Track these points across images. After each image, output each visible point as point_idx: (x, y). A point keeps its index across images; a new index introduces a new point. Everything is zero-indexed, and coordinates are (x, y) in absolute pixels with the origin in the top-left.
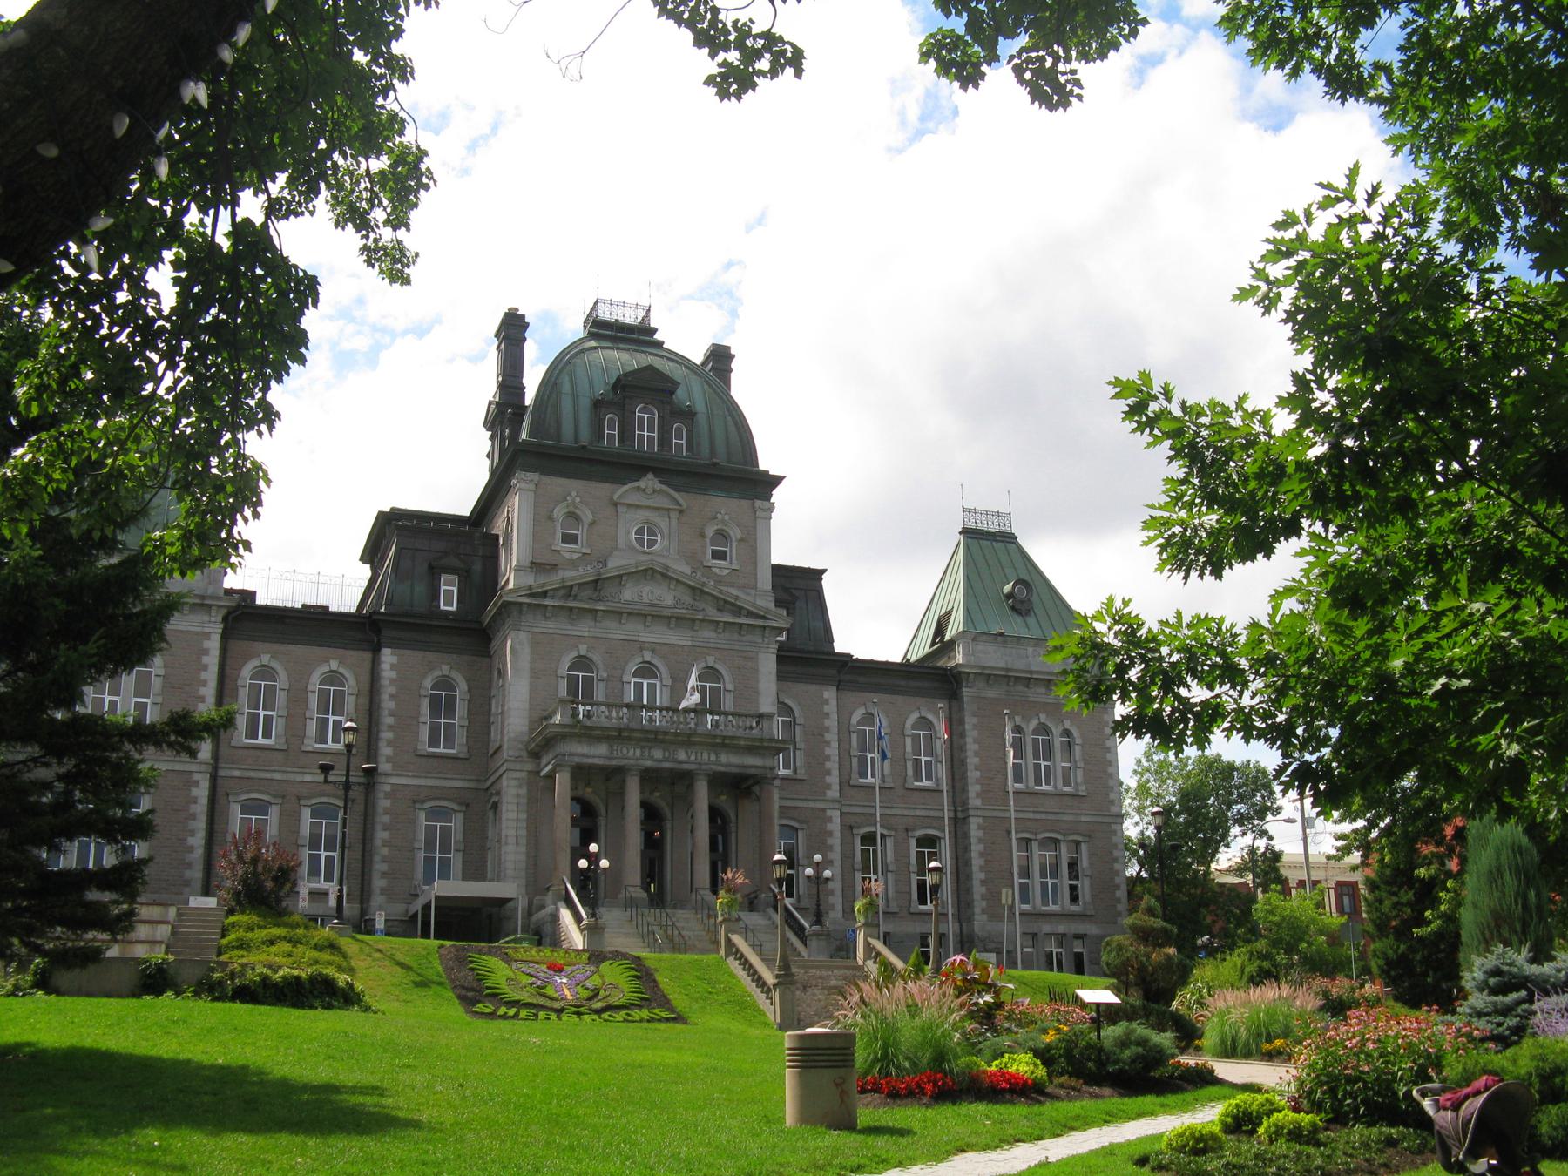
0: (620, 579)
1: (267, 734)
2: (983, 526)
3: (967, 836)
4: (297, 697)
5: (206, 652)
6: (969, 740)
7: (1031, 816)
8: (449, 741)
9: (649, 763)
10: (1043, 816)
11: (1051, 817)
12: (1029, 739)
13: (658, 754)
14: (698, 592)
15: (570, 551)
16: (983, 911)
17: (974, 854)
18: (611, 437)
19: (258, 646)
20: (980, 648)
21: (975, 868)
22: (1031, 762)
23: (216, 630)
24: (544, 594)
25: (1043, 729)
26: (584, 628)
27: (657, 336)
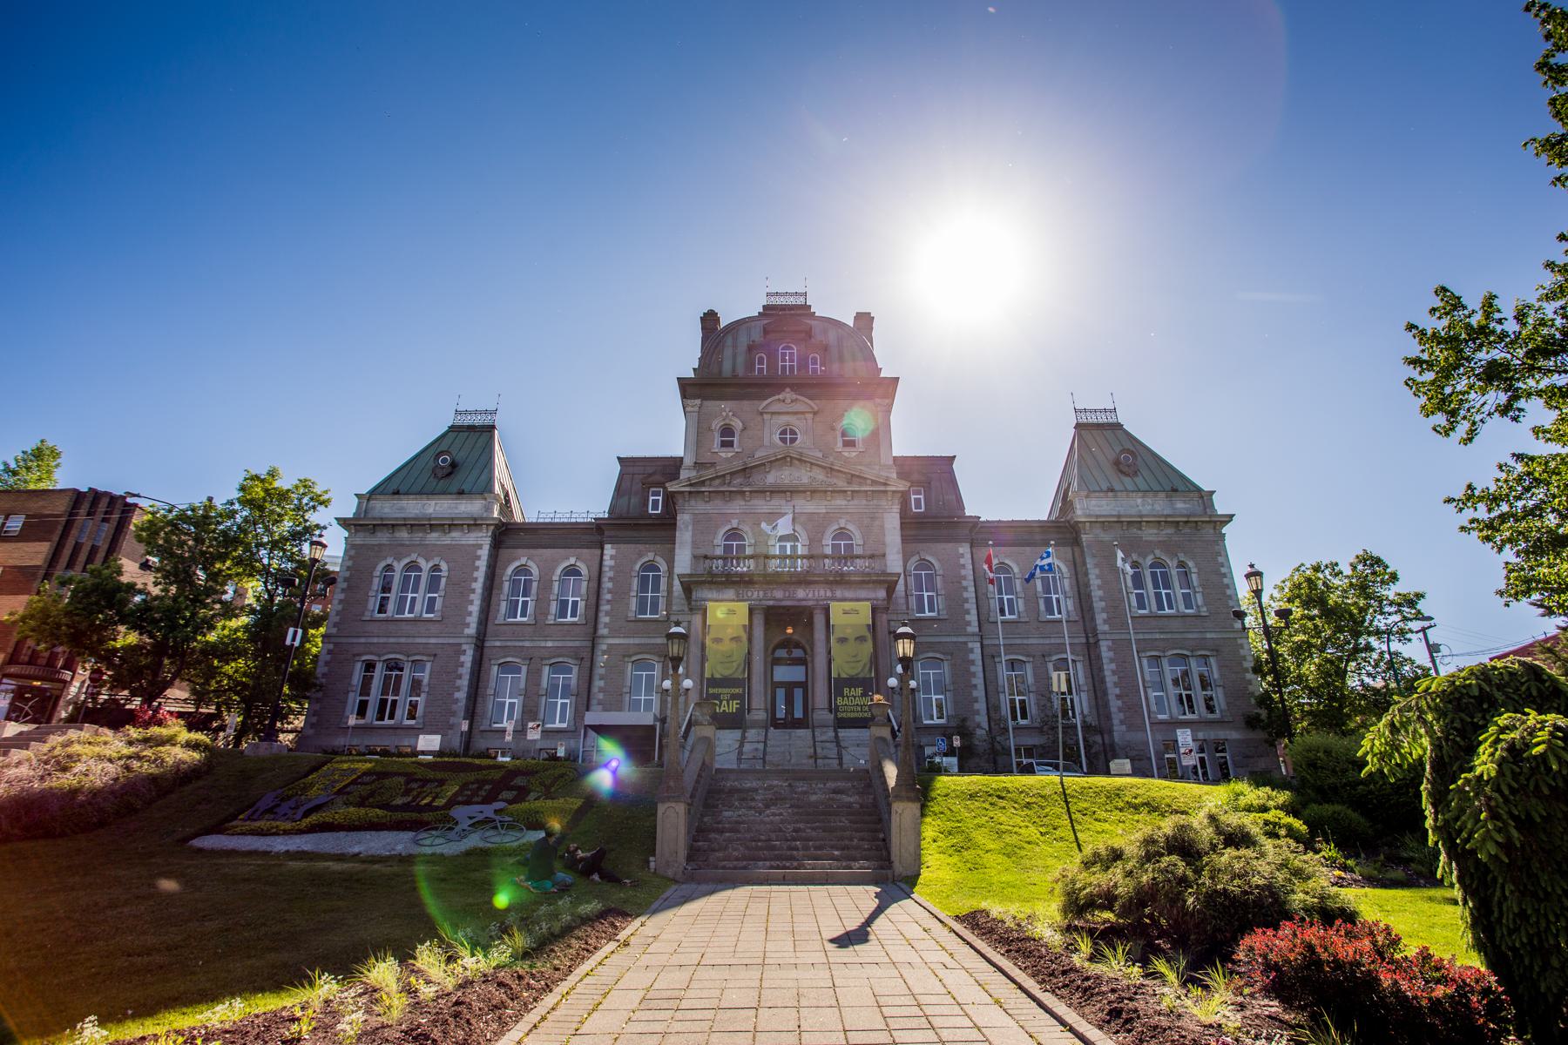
1: (1024, 716)
2: (1092, 419)
3: (1099, 657)
4: (545, 584)
5: (479, 558)
6: (1092, 576)
8: (655, 610)
12: (1147, 573)
13: (779, 594)
15: (726, 454)
16: (1122, 722)
17: (1107, 673)
18: (761, 370)
19: (520, 551)
21: (1109, 685)
23: (486, 543)
24: (703, 483)
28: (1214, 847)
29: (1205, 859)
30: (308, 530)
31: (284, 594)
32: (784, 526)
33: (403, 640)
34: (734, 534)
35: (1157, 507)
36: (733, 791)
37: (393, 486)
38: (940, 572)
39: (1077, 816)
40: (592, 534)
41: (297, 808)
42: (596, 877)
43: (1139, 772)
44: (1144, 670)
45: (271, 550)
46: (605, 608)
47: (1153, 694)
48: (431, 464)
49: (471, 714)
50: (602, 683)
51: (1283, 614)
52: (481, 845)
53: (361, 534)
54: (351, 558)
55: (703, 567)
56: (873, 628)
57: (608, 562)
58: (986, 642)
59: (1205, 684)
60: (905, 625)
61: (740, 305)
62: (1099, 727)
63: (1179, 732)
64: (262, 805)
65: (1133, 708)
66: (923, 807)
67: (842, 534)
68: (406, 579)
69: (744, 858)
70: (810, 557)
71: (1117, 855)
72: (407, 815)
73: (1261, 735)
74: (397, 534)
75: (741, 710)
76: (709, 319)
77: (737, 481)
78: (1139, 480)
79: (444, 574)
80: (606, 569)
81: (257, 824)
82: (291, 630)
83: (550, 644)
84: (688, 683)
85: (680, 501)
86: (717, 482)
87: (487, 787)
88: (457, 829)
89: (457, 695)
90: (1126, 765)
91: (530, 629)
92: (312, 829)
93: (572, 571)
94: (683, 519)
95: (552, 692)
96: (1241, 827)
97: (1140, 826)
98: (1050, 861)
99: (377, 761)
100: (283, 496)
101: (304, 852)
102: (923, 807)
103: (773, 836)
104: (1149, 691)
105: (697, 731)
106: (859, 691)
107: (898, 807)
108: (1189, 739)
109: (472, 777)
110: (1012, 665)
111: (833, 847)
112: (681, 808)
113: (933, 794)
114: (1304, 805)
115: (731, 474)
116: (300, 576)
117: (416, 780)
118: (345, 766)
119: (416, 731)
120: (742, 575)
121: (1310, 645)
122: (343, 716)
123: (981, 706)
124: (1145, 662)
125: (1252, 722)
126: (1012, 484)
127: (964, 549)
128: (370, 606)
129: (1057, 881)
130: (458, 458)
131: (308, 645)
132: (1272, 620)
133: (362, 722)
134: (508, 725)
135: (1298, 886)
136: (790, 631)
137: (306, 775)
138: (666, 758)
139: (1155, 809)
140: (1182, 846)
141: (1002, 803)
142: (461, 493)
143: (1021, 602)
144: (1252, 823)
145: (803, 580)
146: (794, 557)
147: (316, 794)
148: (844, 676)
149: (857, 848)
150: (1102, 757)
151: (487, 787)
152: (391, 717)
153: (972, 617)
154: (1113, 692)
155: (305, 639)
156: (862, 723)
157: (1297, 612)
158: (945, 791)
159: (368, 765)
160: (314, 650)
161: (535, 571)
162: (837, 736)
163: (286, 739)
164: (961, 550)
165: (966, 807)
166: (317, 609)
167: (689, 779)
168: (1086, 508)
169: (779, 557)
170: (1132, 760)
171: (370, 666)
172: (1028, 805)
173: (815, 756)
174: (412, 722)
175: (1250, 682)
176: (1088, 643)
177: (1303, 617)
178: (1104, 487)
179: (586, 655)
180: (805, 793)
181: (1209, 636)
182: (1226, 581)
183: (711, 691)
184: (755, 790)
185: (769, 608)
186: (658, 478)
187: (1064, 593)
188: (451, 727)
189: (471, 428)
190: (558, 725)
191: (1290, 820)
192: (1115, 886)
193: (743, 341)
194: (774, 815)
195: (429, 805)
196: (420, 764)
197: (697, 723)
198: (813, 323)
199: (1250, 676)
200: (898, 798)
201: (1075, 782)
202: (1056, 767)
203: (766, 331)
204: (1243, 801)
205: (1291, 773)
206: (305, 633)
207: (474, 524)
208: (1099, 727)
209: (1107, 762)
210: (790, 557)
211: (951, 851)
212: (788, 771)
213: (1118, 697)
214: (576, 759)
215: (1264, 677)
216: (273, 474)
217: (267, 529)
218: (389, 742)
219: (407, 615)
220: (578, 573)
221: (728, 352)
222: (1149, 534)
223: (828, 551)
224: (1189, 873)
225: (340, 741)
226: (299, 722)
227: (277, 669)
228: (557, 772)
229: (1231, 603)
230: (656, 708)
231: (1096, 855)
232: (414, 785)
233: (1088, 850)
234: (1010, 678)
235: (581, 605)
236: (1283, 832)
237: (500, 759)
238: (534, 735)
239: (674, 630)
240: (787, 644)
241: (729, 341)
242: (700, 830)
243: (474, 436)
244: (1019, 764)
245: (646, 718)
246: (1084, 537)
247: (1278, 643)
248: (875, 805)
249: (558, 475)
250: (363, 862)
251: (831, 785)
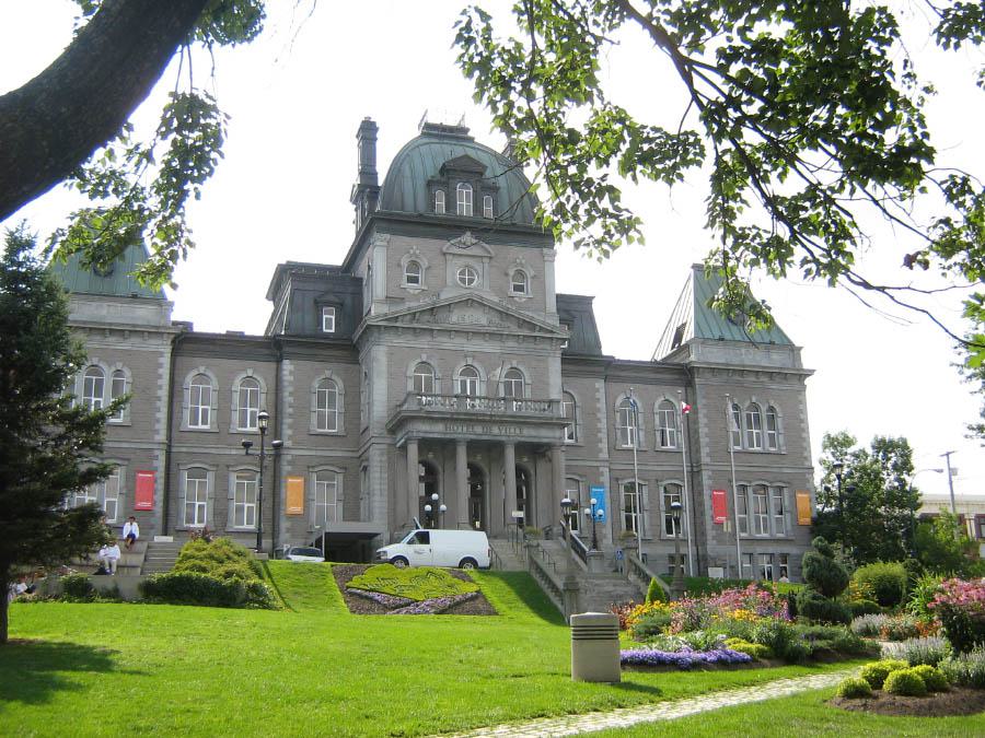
0: (449, 307)
3: (700, 484)
6: (700, 415)
13: (479, 429)
14: (505, 315)
16: (714, 538)
19: (197, 360)
23: (167, 350)
26: (424, 342)
27: (470, 134)
83: (234, 452)
136: (525, 460)
164: (597, 385)
182: (806, 454)
185: (519, 442)
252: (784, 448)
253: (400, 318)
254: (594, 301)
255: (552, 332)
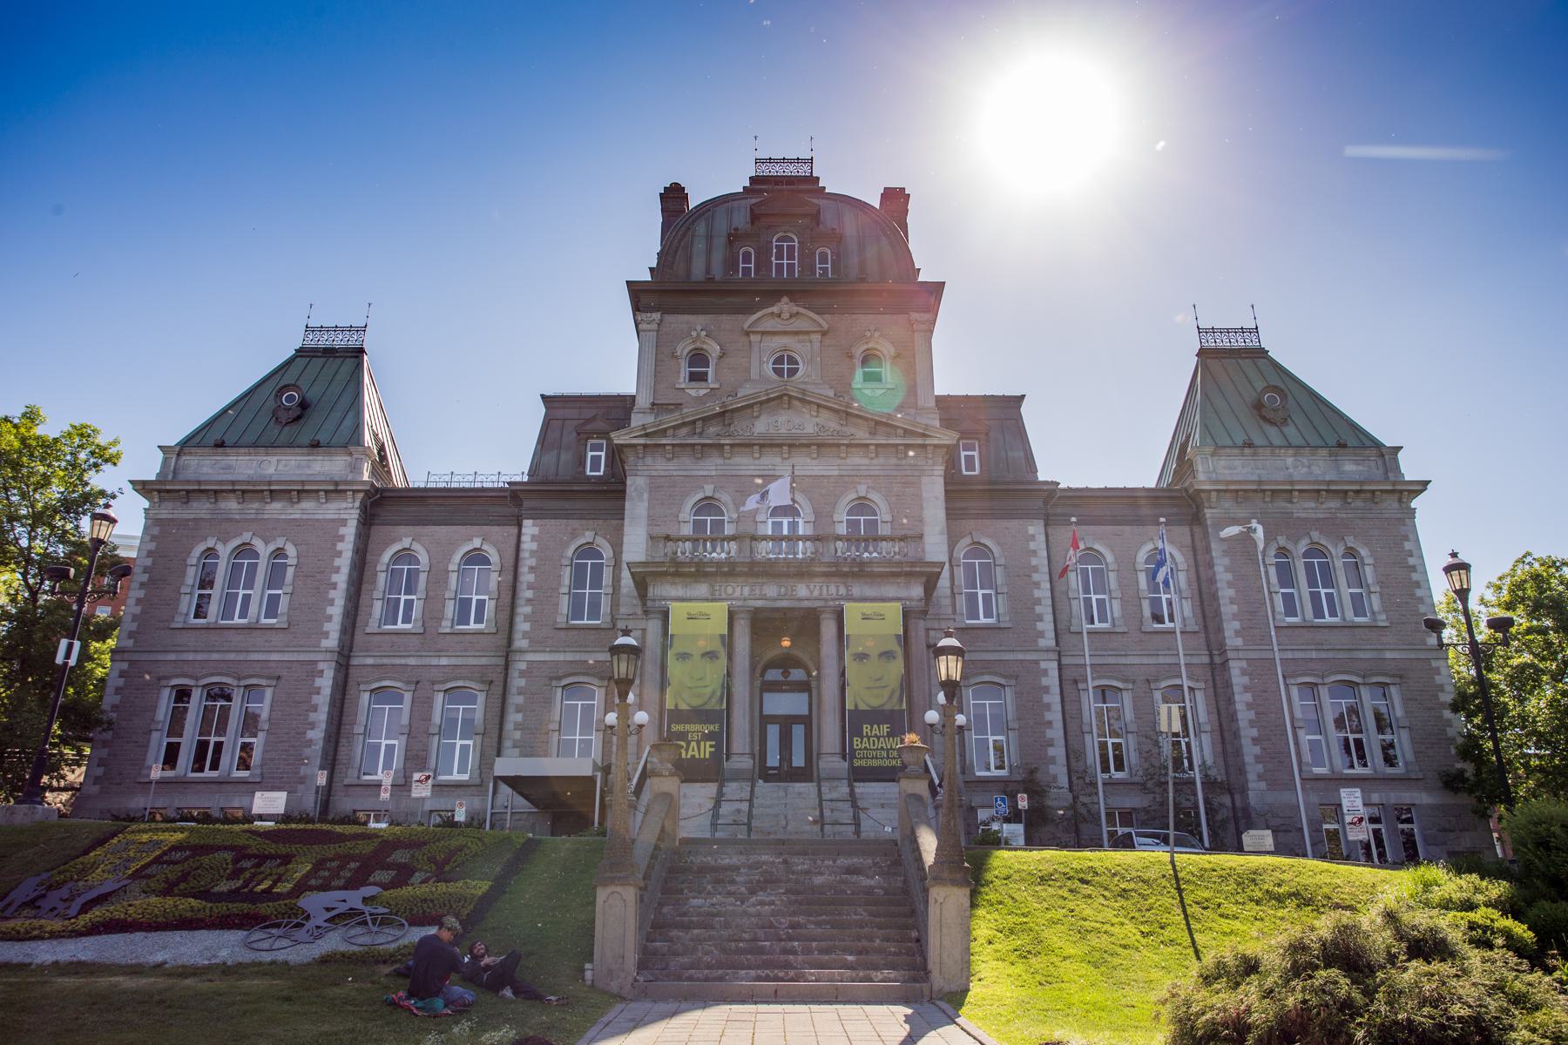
1: (1119, 766)
2: (1224, 342)
3: (1228, 684)
4: (438, 576)
5: (342, 538)
6: (1219, 569)
7: (1314, 655)
8: (594, 613)
9: (759, 604)
10: (1330, 655)
11: (1341, 655)
13: (771, 590)
16: (1260, 777)
17: (1240, 707)
18: (747, 271)
19: (402, 529)
20: (1223, 463)
21: (1243, 724)
22: (1305, 590)
24: (663, 433)
25: (1314, 551)
28: (1392, 959)
29: (1380, 975)
30: (88, 498)
31: (52, 592)
32: (779, 493)
33: (232, 656)
34: (708, 505)
35: (1316, 470)
36: (704, 870)
37: (215, 435)
38: (1002, 561)
39: (1194, 910)
40: (504, 505)
41: (71, 899)
42: (508, 992)
43: (1288, 846)
44: (1294, 704)
45: (33, 528)
46: (524, 609)
47: (1306, 738)
48: (271, 404)
49: (331, 761)
50: (519, 717)
51: (1500, 625)
52: (343, 947)
53: (170, 505)
54: (153, 538)
55: (662, 552)
56: (905, 640)
57: (528, 545)
58: (1065, 661)
59: (1382, 724)
60: (948, 635)
61: (716, 176)
62: (1226, 784)
63: (1344, 792)
64: (19, 896)
65: (1276, 758)
66: (974, 894)
67: (862, 506)
68: (236, 569)
69: (720, 965)
70: (816, 539)
71: (1250, 967)
72: (236, 907)
73: (1465, 799)
74: (223, 505)
75: (717, 756)
76: (673, 196)
77: (713, 430)
78: (1290, 430)
79: (292, 561)
80: (525, 555)
81: (11, 924)
82: (64, 643)
83: (444, 661)
84: (641, 717)
85: (630, 458)
86: (684, 431)
87: (353, 865)
88: (309, 925)
89: (311, 734)
90: (1267, 838)
91: (415, 641)
92: (94, 930)
93: (476, 558)
94: (636, 484)
95: (448, 728)
96: (1433, 931)
97: (1285, 925)
98: (1156, 974)
99: (191, 830)
100: (49, 448)
101: (80, 963)
102: (974, 894)
103: (761, 933)
104: (1301, 733)
105: (653, 785)
106: (885, 728)
107: (937, 893)
108: (1359, 803)
109: (331, 850)
110: (1103, 693)
111: (846, 950)
112: (630, 893)
113: (989, 876)
114: (1530, 904)
115: (704, 419)
116: (78, 565)
117: (249, 857)
118: (145, 837)
119: (251, 787)
120: (719, 564)
121: (1538, 671)
122: (141, 765)
123: (1058, 751)
124: (1295, 691)
125: (1452, 782)
126: (1106, 433)
127: (1036, 529)
128: (183, 607)
129: (1164, 1002)
130: (312, 393)
131: (89, 666)
132: (1483, 634)
133: (170, 774)
134: (385, 777)
135: (1519, 1018)
136: (786, 643)
137: (86, 853)
138: (608, 824)
139: (1308, 902)
140: (1346, 955)
141: (1088, 890)
142: (315, 445)
143: (1116, 604)
144: (1450, 926)
145: (802, 571)
146: (793, 538)
147: (101, 879)
148: (862, 707)
149: (880, 951)
150: (1231, 826)
151: (353, 865)
152: (214, 766)
153: (1047, 626)
154: (1248, 733)
155: (85, 656)
156: (887, 775)
157: (1521, 620)
158: (1005, 872)
159: (179, 836)
160: (99, 672)
161: (423, 558)
162: (852, 793)
163: (57, 800)
164: (1031, 530)
165: (1035, 895)
166: (103, 613)
167: (641, 854)
168: (1209, 471)
169: (772, 538)
170: (1275, 832)
171: (183, 694)
172: (1124, 894)
173: (821, 821)
174: (244, 774)
175: (1449, 723)
176: (1212, 663)
177: (1529, 631)
178: (1239, 442)
179: (497, 677)
180: (807, 872)
181: (1388, 655)
182: (1415, 577)
183: (676, 728)
184: (736, 868)
185: (757, 610)
186: (600, 425)
187: (1179, 591)
188: (302, 780)
189: (329, 352)
190: (455, 776)
191: (1508, 922)
192: (1248, 1011)
193: (721, 226)
194: (762, 903)
195: (267, 891)
196: (255, 833)
197: (655, 774)
198: (821, 202)
199: (1447, 714)
200: (938, 880)
201: (1191, 861)
202: (1166, 840)
203: (755, 217)
204: (1437, 894)
205: (1510, 853)
206: (85, 647)
207: (335, 490)
208: (1226, 784)
209: (1239, 835)
210: (788, 539)
211: (1013, 957)
212: (783, 842)
213: (1255, 741)
214: (481, 824)
215: (1469, 717)
216: (31, 416)
217: (24, 496)
218: (213, 802)
219: (237, 620)
220: (486, 561)
221: (699, 246)
222: (1304, 509)
223: (842, 530)
224: (1356, 995)
225: (138, 802)
226: (76, 776)
227: (43, 699)
228: (454, 843)
229: (1422, 609)
230: (596, 753)
231: (1220, 965)
232: (247, 864)
233: (1209, 959)
234: (1099, 713)
235: (490, 607)
236: (1500, 941)
237: (372, 825)
238: (421, 791)
239: (621, 640)
240: (786, 662)
241: (701, 228)
242: (656, 926)
243: (333, 364)
244: (1112, 834)
245: (580, 766)
246: (1208, 513)
247: (1490, 670)
248: (906, 891)
249: (453, 422)
250: (170, 975)
251: (843, 861)
252: (1384, 617)
253: (670, 432)
254: (1025, 409)
255: (924, 436)
